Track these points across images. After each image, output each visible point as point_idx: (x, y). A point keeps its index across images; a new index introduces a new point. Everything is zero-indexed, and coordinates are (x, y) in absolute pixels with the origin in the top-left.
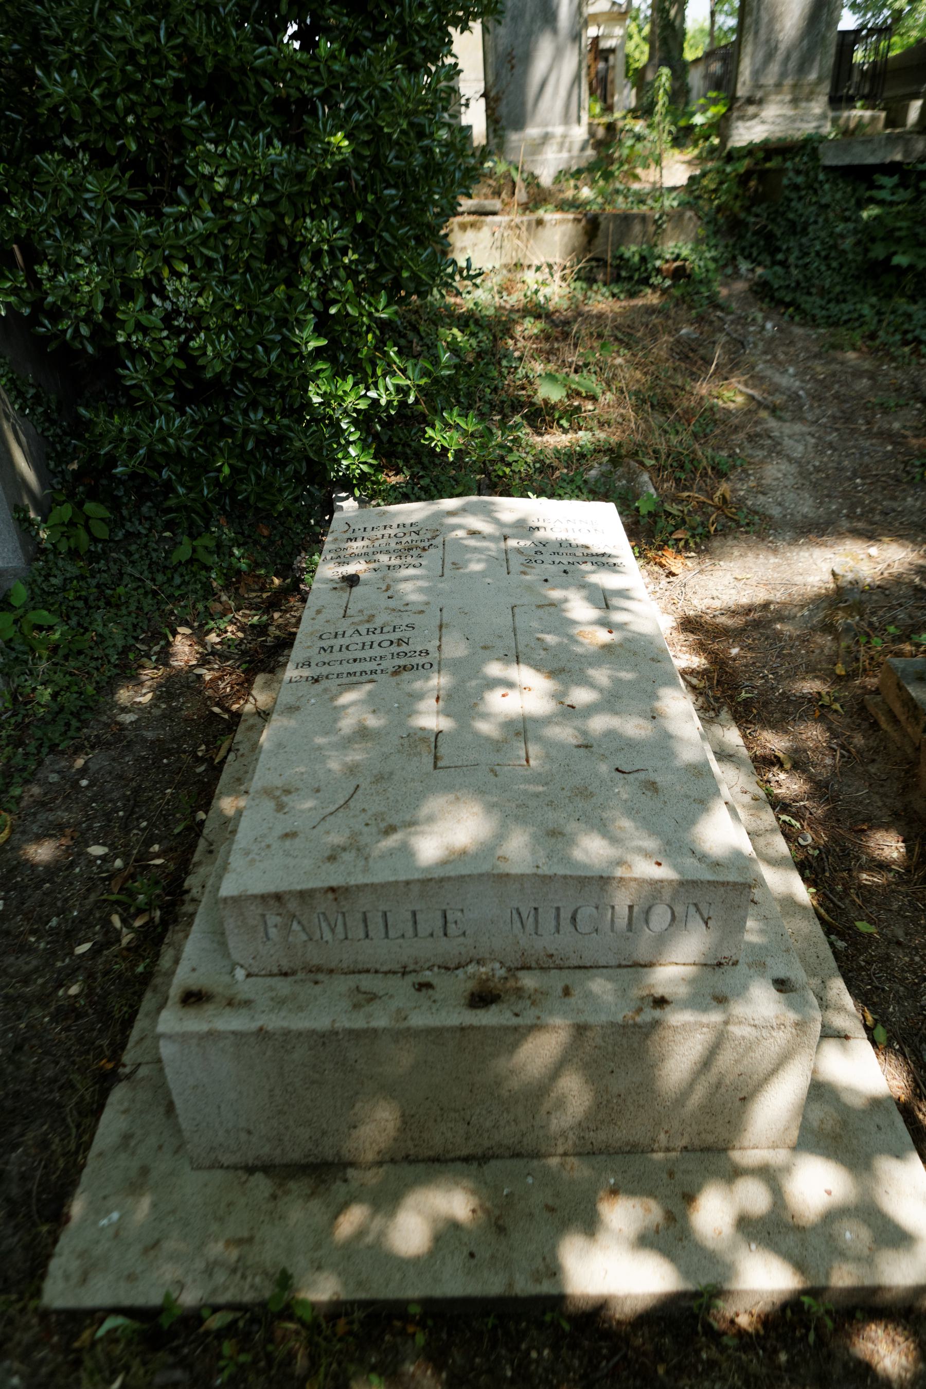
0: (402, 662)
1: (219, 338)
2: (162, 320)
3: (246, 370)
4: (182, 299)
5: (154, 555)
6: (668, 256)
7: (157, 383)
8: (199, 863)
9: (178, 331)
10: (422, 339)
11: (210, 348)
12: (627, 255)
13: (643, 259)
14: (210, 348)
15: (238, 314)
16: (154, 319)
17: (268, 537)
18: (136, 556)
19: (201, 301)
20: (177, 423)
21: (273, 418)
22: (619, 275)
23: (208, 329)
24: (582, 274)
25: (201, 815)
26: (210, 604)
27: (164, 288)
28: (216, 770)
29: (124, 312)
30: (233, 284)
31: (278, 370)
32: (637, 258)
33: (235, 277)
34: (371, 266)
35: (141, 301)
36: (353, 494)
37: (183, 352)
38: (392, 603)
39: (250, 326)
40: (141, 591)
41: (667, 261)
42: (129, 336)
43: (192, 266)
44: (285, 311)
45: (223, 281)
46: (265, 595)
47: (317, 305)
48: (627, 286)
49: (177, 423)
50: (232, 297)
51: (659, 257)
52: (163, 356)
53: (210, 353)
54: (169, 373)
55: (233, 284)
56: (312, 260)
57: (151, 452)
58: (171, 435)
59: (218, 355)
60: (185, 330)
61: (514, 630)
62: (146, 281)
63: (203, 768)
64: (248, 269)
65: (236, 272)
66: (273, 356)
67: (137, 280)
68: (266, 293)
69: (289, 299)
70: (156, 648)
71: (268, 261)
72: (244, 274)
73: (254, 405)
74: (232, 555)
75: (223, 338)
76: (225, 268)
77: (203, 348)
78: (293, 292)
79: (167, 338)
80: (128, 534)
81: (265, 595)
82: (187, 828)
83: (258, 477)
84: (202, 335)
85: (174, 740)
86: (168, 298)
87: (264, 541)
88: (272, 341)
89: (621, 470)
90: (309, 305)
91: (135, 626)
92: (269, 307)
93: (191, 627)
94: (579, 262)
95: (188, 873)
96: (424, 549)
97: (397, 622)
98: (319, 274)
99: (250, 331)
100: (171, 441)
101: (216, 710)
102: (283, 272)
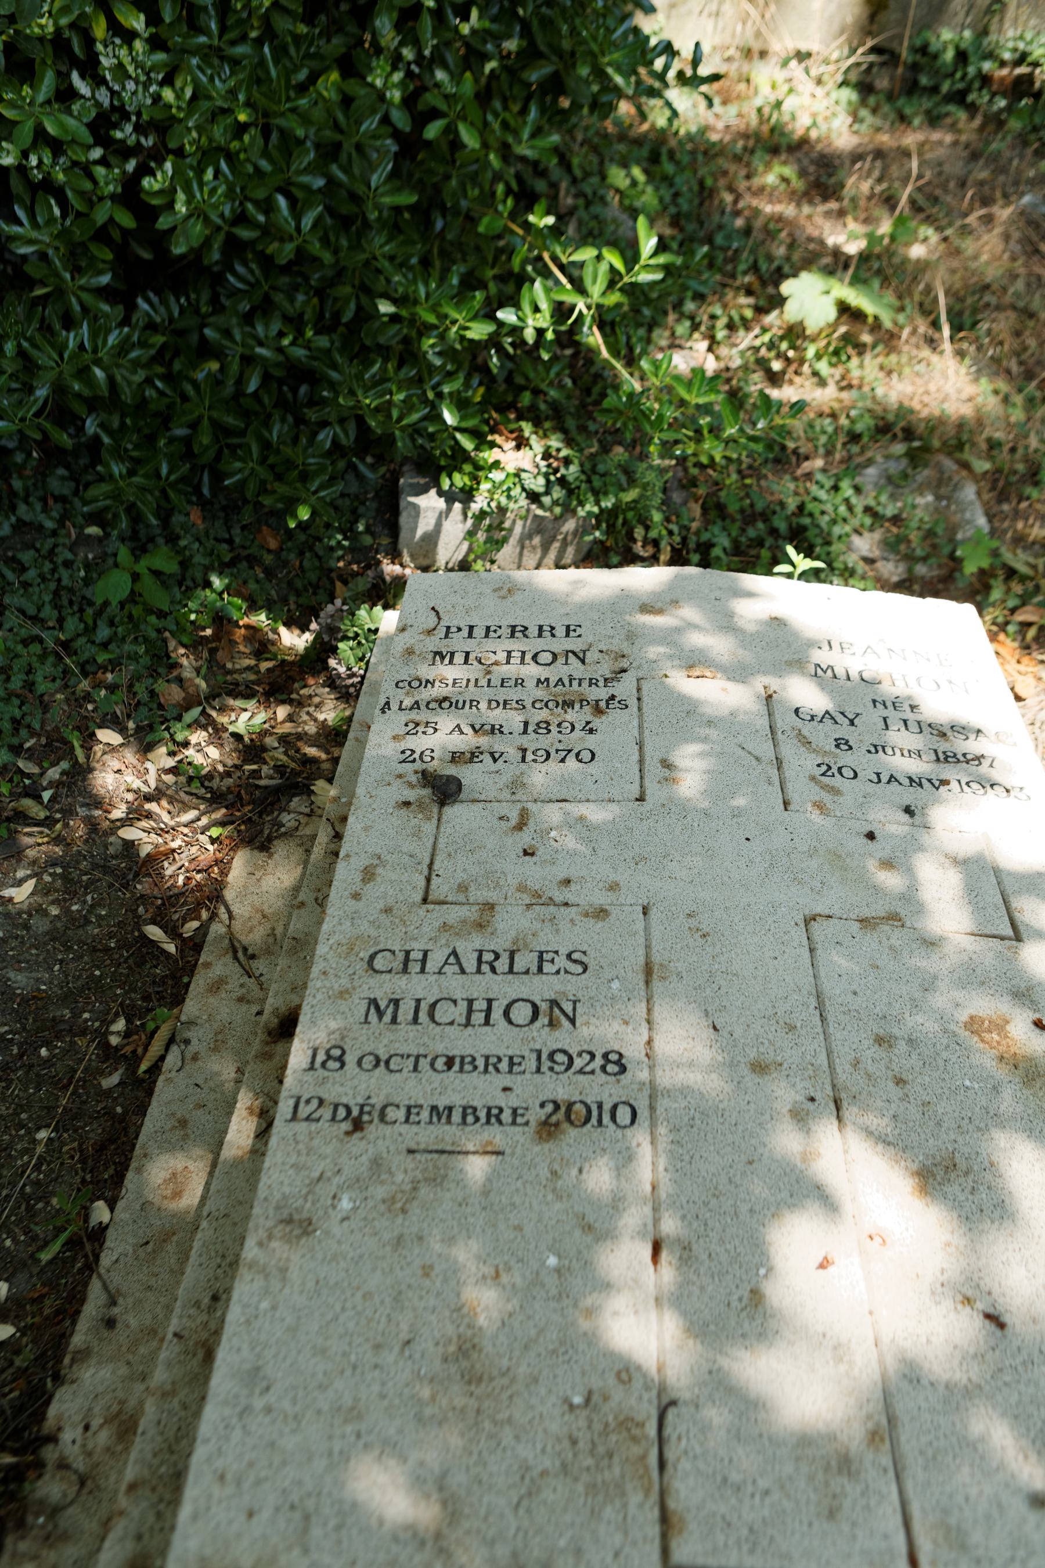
0: (561, 1088)
1: (200, 172)
2: (90, 126)
3: (252, 243)
4: (131, 86)
5: (65, 574)
6: (1007, 56)
7: (77, 258)
8: (83, 1355)
9: (125, 152)
10: (574, 181)
11: (181, 196)
12: (934, 46)
13: (962, 56)
14: (181, 196)
15: (241, 129)
16: (72, 124)
17: (278, 553)
18: (31, 574)
19: (168, 95)
20: (112, 340)
21: (300, 333)
22: (915, 83)
23: (179, 153)
24: (853, 77)
25: (101, 1212)
26: (160, 686)
27: (93, 60)
28: (141, 1088)
29: (12, 104)
30: (235, 63)
31: (315, 247)
32: (949, 55)
33: (240, 50)
34: (511, 45)
35: (48, 82)
36: (437, 484)
37: (130, 194)
38: (533, 873)
39: (265, 154)
40: (35, 648)
41: (1003, 64)
42: (25, 155)
43: (153, 19)
44: (336, 127)
45: (212, 55)
46: (265, 666)
47: (400, 119)
48: (927, 103)
49: (112, 340)
50: (232, 93)
51: (990, 55)
52: (92, 200)
53: (181, 208)
54: (102, 235)
55: (235, 63)
56: (398, 27)
57: (59, 389)
58: (98, 362)
59: (197, 212)
60: (137, 149)
61: (821, 1007)
62: (59, 43)
63: (115, 1079)
64: (269, 32)
65: (244, 38)
66: (307, 222)
67: (41, 39)
68: (302, 88)
69: (347, 101)
70: (54, 773)
71: (308, 19)
72: (259, 42)
73: (264, 308)
74: (208, 584)
75: (209, 174)
76: (223, 29)
77: (169, 193)
78: (353, 87)
79: (103, 162)
80: (21, 526)
81: (265, 666)
82: (73, 1243)
83: (266, 445)
84: (168, 166)
85: (67, 998)
86: (103, 81)
87: (268, 559)
88: (306, 188)
89: (924, 474)
90: (386, 120)
91: (16, 723)
92: (305, 119)
93: (122, 730)
94: (853, 51)
95: (58, 1379)
96: (598, 711)
97: (546, 940)
98: (408, 53)
99: (265, 165)
100: (99, 373)
101: (154, 932)
102: (337, 45)
